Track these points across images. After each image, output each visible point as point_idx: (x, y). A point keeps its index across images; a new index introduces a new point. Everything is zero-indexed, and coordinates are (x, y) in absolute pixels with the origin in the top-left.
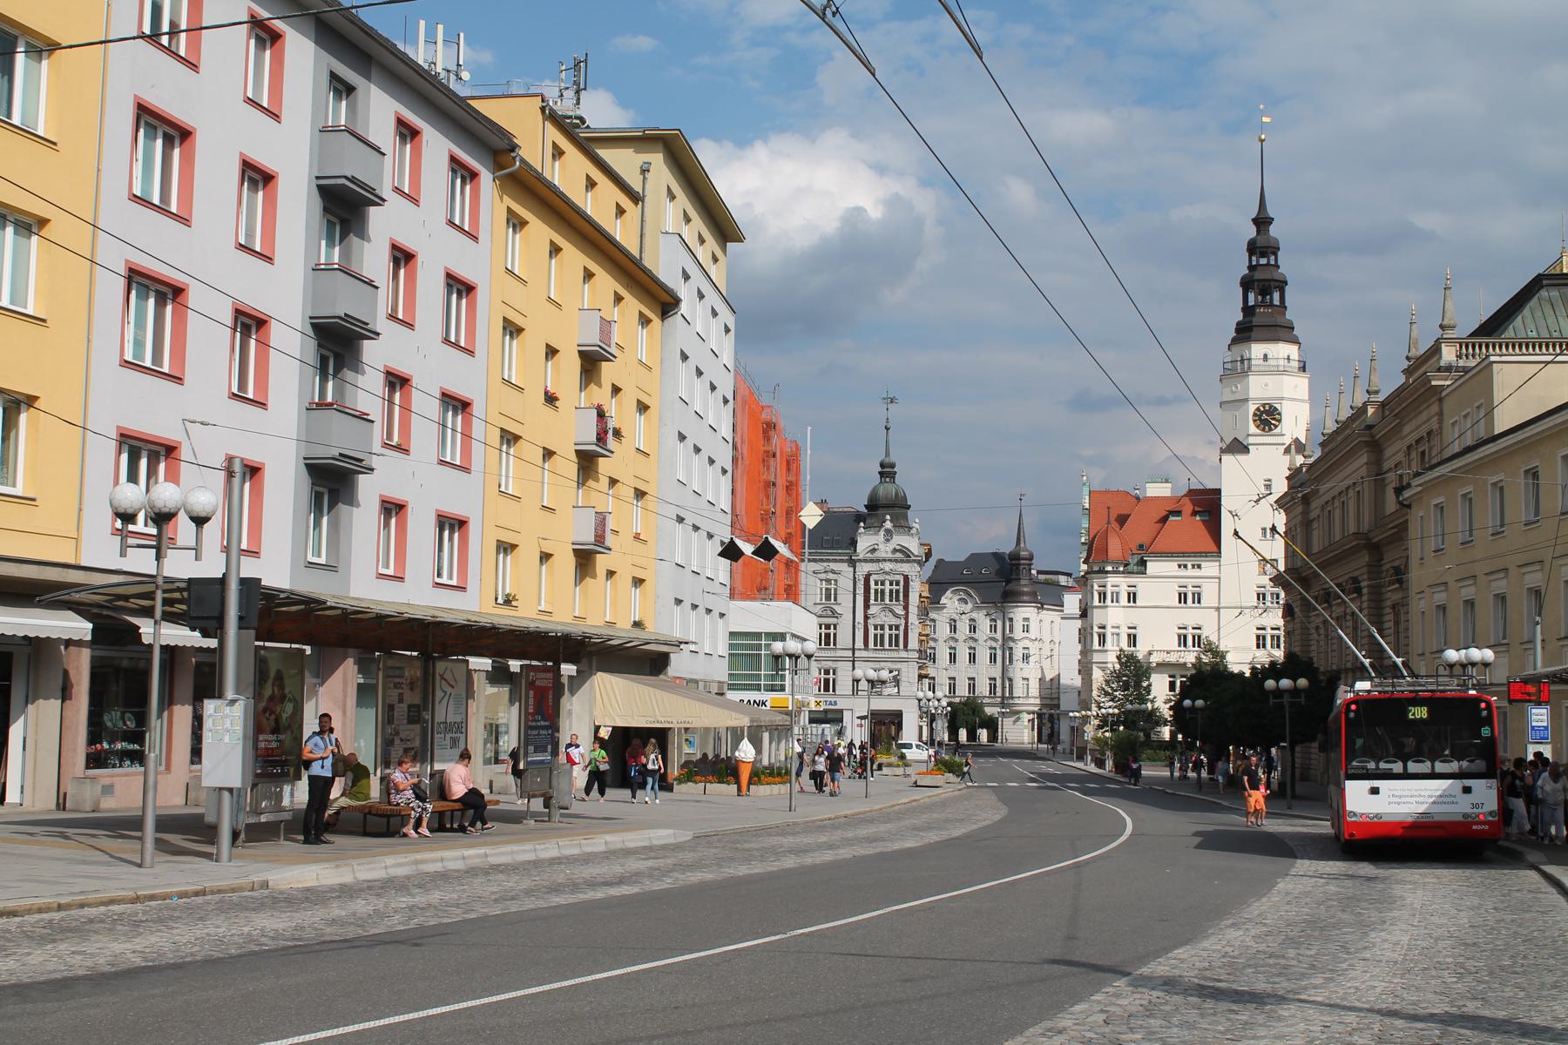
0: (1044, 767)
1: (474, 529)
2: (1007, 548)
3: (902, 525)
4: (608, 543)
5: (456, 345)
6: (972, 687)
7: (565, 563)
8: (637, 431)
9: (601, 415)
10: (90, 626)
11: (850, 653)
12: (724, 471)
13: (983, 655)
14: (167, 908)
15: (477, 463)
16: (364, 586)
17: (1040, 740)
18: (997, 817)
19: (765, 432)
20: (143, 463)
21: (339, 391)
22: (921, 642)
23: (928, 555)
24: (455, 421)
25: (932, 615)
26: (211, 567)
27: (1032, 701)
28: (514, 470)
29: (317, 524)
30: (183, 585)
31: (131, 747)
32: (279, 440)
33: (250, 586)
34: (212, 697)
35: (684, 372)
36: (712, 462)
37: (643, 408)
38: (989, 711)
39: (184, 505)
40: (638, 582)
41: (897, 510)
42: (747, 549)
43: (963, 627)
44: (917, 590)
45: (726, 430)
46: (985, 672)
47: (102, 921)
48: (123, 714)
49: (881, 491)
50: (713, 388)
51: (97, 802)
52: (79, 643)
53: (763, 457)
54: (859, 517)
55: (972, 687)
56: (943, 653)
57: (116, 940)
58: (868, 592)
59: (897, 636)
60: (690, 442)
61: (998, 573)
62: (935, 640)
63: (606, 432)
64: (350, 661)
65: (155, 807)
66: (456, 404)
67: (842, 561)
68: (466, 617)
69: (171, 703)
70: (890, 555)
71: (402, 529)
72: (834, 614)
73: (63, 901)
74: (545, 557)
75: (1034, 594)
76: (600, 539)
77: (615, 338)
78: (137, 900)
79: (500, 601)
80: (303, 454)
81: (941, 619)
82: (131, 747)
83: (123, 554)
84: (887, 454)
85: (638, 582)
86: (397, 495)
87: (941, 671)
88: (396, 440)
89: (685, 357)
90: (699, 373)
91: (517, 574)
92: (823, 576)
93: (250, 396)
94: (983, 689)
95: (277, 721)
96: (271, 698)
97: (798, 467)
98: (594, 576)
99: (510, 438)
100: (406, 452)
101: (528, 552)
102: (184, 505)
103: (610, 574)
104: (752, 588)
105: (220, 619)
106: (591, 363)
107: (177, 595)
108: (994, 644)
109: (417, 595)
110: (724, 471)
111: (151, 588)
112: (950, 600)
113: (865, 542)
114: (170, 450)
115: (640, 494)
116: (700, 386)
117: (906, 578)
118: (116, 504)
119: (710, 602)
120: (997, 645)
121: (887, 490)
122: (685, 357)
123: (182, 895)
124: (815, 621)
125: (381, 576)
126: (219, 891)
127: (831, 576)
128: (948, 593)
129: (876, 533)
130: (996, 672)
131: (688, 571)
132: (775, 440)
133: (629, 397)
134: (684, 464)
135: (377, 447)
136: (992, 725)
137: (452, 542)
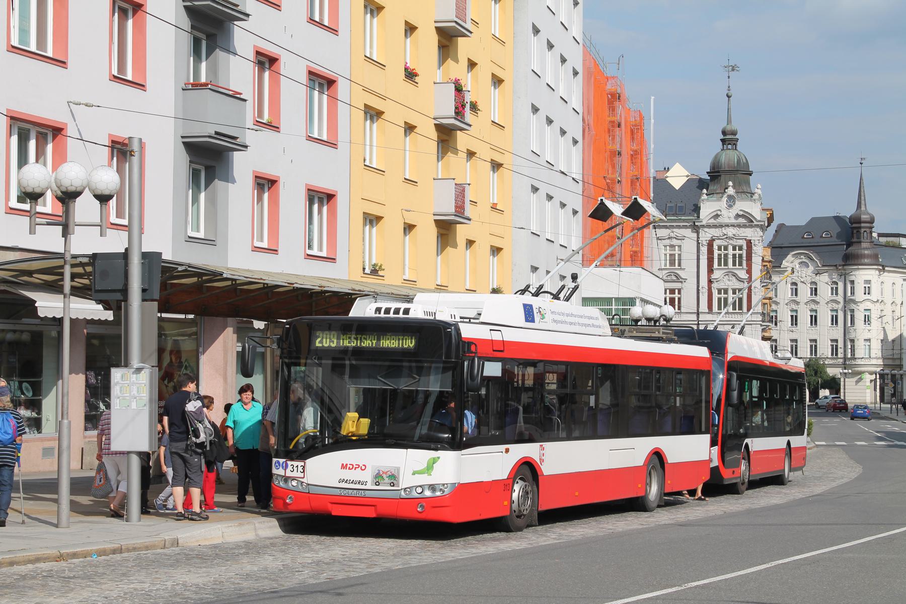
0: (889, 426)
1: (341, 201)
2: (848, 211)
3: (745, 192)
4: (467, 213)
5: (320, 24)
6: (814, 349)
7: (428, 233)
8: (493, 105)
9: (459, 90)
11: (694, 317)
12: (575, 142)
13: (825, 317)
14: (91, 565)
16: (241, 258)
17: (882, 400)
18: (854, 475)
19: (610, 103)
20: (32, 144)
23: (770, 220)
24: (320, 100)
25: (775, 278)
27: (874, 362)
28: (378, 142)
29: (195, 200)
30: (86, 260)
33: (151, 259)
34: (118, 365)
35: (536, 44)
36: (563, 132)
37: (497, 81)
38: (831, 372)
39: (662, 316)
40: (496, 251)
43: (805, 292)
44: (760, 252)
45: (576, 102)
46: (827, 334)
47: (34, 578)
48: (20, 383)
49: (723, 159)
50: (563, 60)
53: (610, 124)
55: (814, 349)
56: (785, 315)
57: (51, 595)
58: (712, 257)
59: (740, 300)
61: (839, 236)
62: (777, 303)
63: (463, 106)
64: (229, 331)
65: (69, 471)
66: (322, 82)
67: (685, 227)
68: (319, 283)
70: (733, 221)
72: (679, 279)
74: (409, 228)
75: (876, 257)
76: (460, 209)
77: (471, 14)
78: (60, 558)
79: (368, 271)
80: (181, 133)
83: (32, 231)
84: (729, 121)
85: (496, 251)
86: (269, 171)
88: (266, 118)
89: (536, 31)
90: (550, 46)
91: (379, 245)
92: (668, 242)
93: (129, 78)
94: (824, 350)
97: (642, 136)
98: (455, 246)
100: (276, 128)
101: (393, 224)
102: (88, 185)
103: (470, 243)
105: (125, 291)
106: (448, 38)
107: (80, 270)
108: (835, 306)
109: (290, 265)
110: (575, 142)
111: (59, 262)
112: (790, 262)
113: (708, 207)
114: (57, 131)
115: (496, 166)
116: (551, 58)
117: (749, 243)
118: (24, 183)
121: (729, 157)
122: (536, 31)
124: (661, 285)
126: (134, 549)
127: (675, 242)
129: (720, 199)
130: (838, 333)
132: (620, 110)
133: (484, 71)
134: (538, 138)
135: (250, 123)
136: (834, 385)
137: (321, 215)
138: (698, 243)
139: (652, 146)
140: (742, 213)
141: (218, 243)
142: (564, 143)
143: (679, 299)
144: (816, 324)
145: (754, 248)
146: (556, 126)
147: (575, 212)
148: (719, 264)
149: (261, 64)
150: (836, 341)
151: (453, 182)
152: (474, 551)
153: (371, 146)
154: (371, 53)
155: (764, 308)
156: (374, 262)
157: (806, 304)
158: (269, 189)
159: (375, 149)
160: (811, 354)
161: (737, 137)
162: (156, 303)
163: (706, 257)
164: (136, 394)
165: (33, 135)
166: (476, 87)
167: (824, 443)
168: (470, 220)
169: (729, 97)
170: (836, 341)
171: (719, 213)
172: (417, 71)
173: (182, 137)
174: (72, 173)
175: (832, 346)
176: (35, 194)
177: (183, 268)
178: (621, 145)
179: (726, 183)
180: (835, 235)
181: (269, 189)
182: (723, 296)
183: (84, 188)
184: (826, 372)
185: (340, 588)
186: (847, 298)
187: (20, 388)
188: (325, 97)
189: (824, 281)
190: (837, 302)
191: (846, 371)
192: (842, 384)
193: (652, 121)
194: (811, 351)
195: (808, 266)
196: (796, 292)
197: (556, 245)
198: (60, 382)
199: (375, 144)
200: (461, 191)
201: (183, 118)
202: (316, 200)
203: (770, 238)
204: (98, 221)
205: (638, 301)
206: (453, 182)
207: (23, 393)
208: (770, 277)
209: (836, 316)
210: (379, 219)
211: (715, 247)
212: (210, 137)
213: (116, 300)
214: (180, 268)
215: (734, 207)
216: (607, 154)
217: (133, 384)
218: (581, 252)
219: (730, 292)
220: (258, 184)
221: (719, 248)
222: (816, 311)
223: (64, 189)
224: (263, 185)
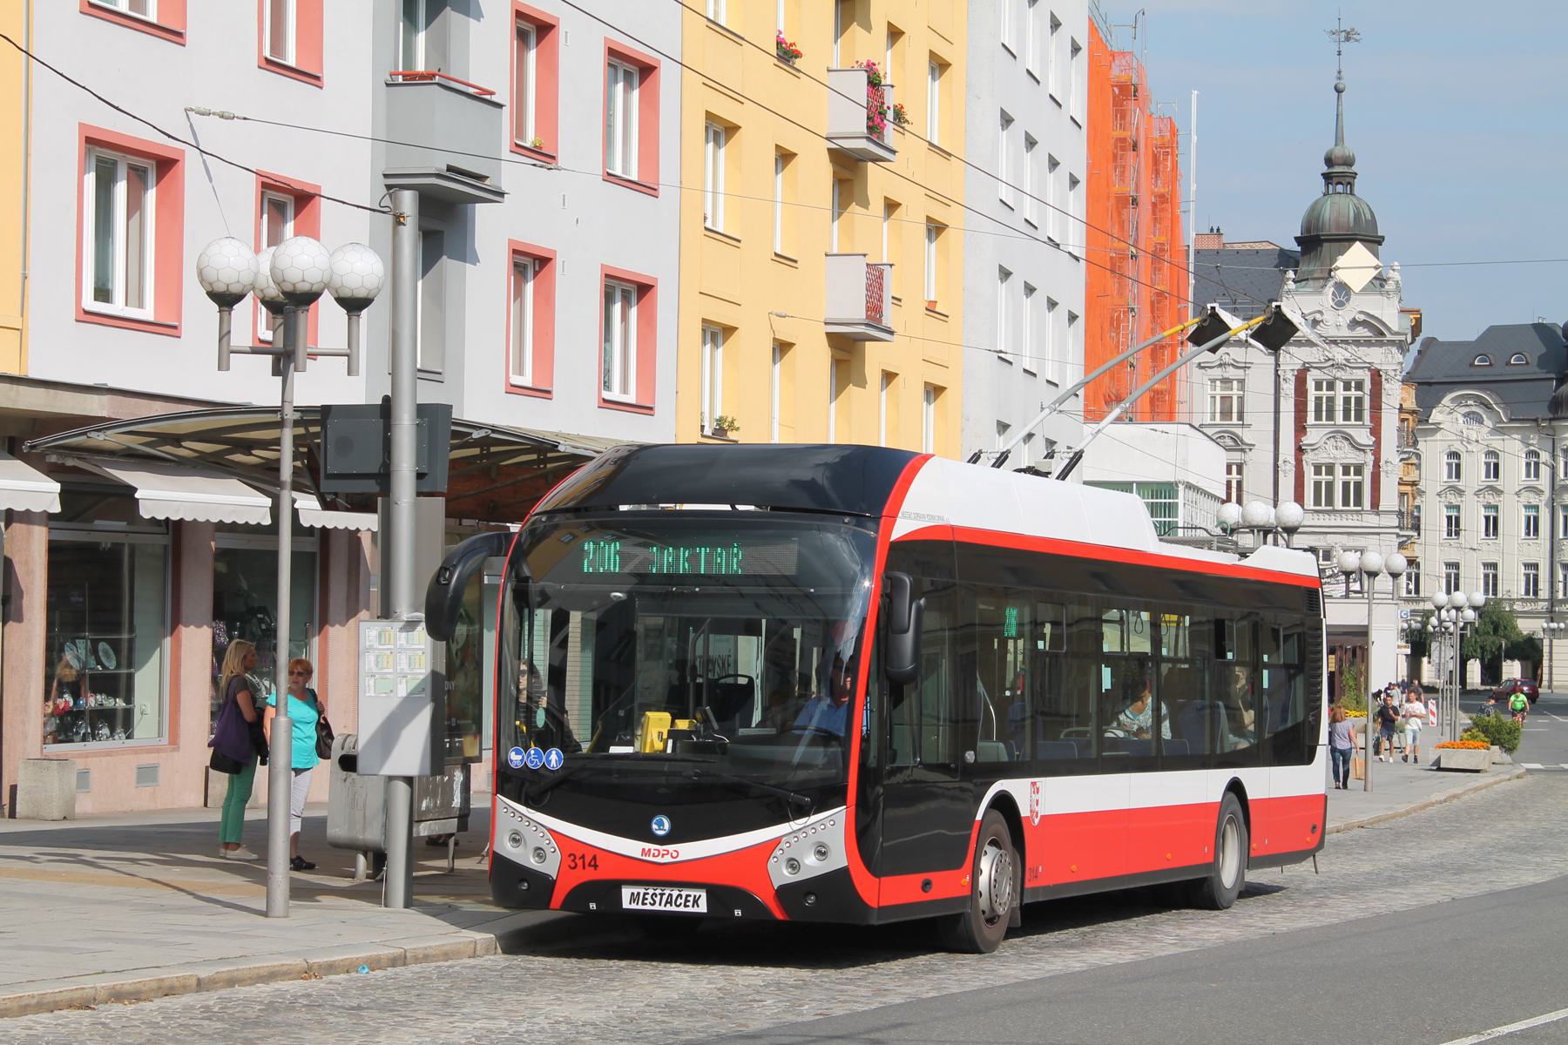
1: (664, 297)
4: (887, 321)
6: (1491, 582)
7: (815, 357)
8: (927, 105)
9: (874, 83)
10: (57, 487)
13: (1513, 519)
15: (667, 175)
21: (439, 48)
22: (1402, 494)
23: (1416, 329)
24: (628, 100)
28: (716, 183)
31: (109, 703)
32: (341, 139)
33: (433, 417)
36: (1054, 164)
37: (939, 66)
38: (1525, 626)
40: (934, 391)
44: (1396, 395)
45: (1077, 105)
48: (95, 643)
49: (1327, 212)
51: (71, 803)
52: (27, 517)
54: (1286, 260)
55: (1491, 582)
56: (1434, 516)
59: (1358, 486)
61: (1543, 362)
62: (1421, 493)
63: (882, 114)
66: (632, 68)
69: (176, 621)
70: (1345, 333)
71: (545, 301)
72: (1238, 445)
73: (205, 973)
74: (782, 348)
76: (874, 310)
78: (308, 972)
79: (708, 431)
81: (1433, 451)
82: (109, 703)
83: (223, 365)
84: (1339, 139)
85: (934, 391)
86: (538, 240)
87: (1434, 550)
88: (530, 139)
93: (291, 61)
94: (1512, 584)
98: (862, 383)
101: (753, 341)
103: (889, 377)
105: (384, 478)
109: (580, 418)
110: (1074, 182)
112: (1448, 416)
114: (166, 165)
117: (1376, 376)
118: (211, 275)
120: (1542, 501)
121: (1338, 210)
123: (375, 964)
125: (515, 389)
127: (1231, 373)
128: (1446, 400)
131: (1017, 369)
132: (1135, 116)
133: (916, 48)
135: (505, 153)
136: (1529, 652)
138: (1277, 376)
139: (1193, 187)
140: (1362, 317)
141: (447, 377)
142: (1055, 184)
144: (1457, 533)
145: (1385, 385)
146: (1041, 151)
147: (1073, 318)
148: (1318, 417)
149: (522, 36)
150: (1536, 566)
151: (863, 261)
153: (715, 193)
154: (716, 13)
155: (1401, 502)
157: (1518, 494)
158: (536, 274)
159: (721, 198)
160: (1486, 591)
161: (1354, 169)
162: (441, 501)
163: (1292, 401)
164: (407, 670)
165: (122, 171)
166: (906, 81)
167: (1538, 766)
168: (892, 333)
169: (1339, 91)
170: (1536, 566)
171: (1318, 317)
172: (798, 48)
173: (386, 176)
175: (1527, 576)
176: (231, 295)
177: (482, 433)
178: (1137, 188)
180: (1533, 360)
181: (536, 274)
182: (1324, 477)
184: (1515, 628)
185: (878, 1030)
186: (1558, 483)
187: (95, 651)
188: (636, 94)
189: (1513, 451)
190: (1538, 492)
191: (1554, 625)
192: (1546, 650)
193: (1194, 138)
194: (1486, 584)
195: (1481, 422)
196: (1457, 472)
197: (1041, 380)
198: (168, 641)
199: (721, 189)
200: (876, 278)
201: (387, 141)
202: (618, 295)
203: (1408, 365)
204: (342, 345)
205: (1181, 488)
206: (863, 261)
207: (99, 662)
208: (1415, 443)
209: (1536, 519)
210: (729, 331)
211: (1311, 385)
212: (438, 176)
213: (371, 493)
214: (476, 435)
215: (1348, 306)
216: (1112, 201)
217: (402, 650)
218: (1081, 393)
219: (1339, 470)
220: (516, 265)
221: (1318, 386)
222: (1496, 508)
223: (288, 288)
224: (525, 267)
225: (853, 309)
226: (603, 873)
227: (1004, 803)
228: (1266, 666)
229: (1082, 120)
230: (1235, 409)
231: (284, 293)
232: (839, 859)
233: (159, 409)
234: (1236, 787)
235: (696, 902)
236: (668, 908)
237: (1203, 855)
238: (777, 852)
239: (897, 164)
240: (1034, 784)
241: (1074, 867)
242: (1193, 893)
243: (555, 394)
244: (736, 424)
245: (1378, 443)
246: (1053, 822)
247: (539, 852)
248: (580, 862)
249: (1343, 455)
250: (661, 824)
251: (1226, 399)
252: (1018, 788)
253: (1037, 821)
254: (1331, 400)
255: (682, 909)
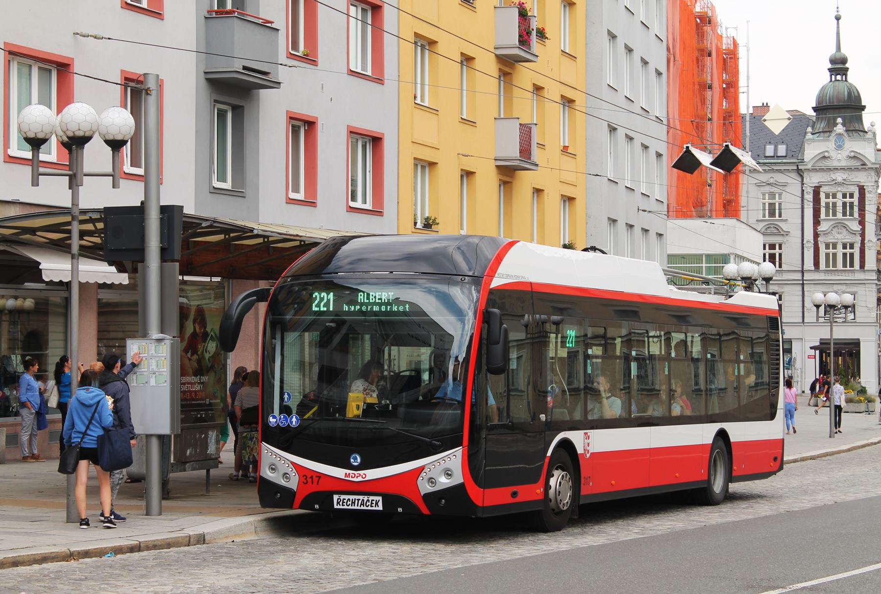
7: (487, 179)
11: (798, 276)
12: (659, 74)
26: (129, 196)
30: (95, 216)
32: (174, 53)
33: (169, 213)
41: (848, 114)
42: (705, 159)
45: (658, 27)
59: (852, 255)
60: (620, 42)
63: (529, 34)
70: (844, 163)
72: (779, 232)
76: (526, 151)
79: (419, 225)
83: (35, 183)
84: (839, 48)
86: (306, 110)
92: (767, 189)
95: (199, 361)
96: (194, 335)
99: (426, 44)
101: (448, 173)
104: (690, 206)
107: (90, 227)
111: (68, 219)
113: (811, 151)
115: (568, 102)
117: (862, 190)
118: (25, 128)
119: (644, 221)
124: (760, 240)
131: (621, 188)
135: (282, 58)
140: (852, 154)
143: (780, 255)
145: (867, 195)
148: (827, 214)
152: (544, 547)
153: (423, 84)
156: (427, 215)
159: (427, 87)
161: (847, 65)
164: (155, 369)
169: (838, 18)
171: (826, 154)
173: (205, 73)
174: (80, 114)
176: (38, 139)
177: (208, 223)
178: (712, 80)
179: (835, 119)
183: (94, 133)
199: (427, 82)
200: (526, 132)
201: (207, 51)
204: (110, 170)
211: (822, 196)
214: (204, 224)
216: (697, 87)
221: (827, 196)
223: (71, 134)
225: (512, 151)
226: (324, 487)
227: (566, 445)
228: (742, 362)
229: (664, 38)
230: (777, 212)
231: (68, 137)
232: (458, 478)
233: (13, 212)
234: (722, 435)
235: (377, 504)
236: (362, 508)
237: (701, 474)
238: (423, 474)
239: (538, 65)
240: (586, 434)
241: (613, 482)
242: (697, 496)
243: (318, 205)
244: (437, 221)
245: (863, 230)
246: (598, 456)
247: (285, 475)
248: (309, 480)
249: (841, 237)
250: (355, 459)
251: (772, 205)
252: (576, 437)
253: (588, 455)
254: (834, 204)
255: (369, 508)
